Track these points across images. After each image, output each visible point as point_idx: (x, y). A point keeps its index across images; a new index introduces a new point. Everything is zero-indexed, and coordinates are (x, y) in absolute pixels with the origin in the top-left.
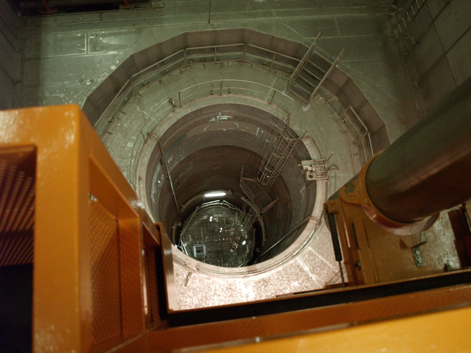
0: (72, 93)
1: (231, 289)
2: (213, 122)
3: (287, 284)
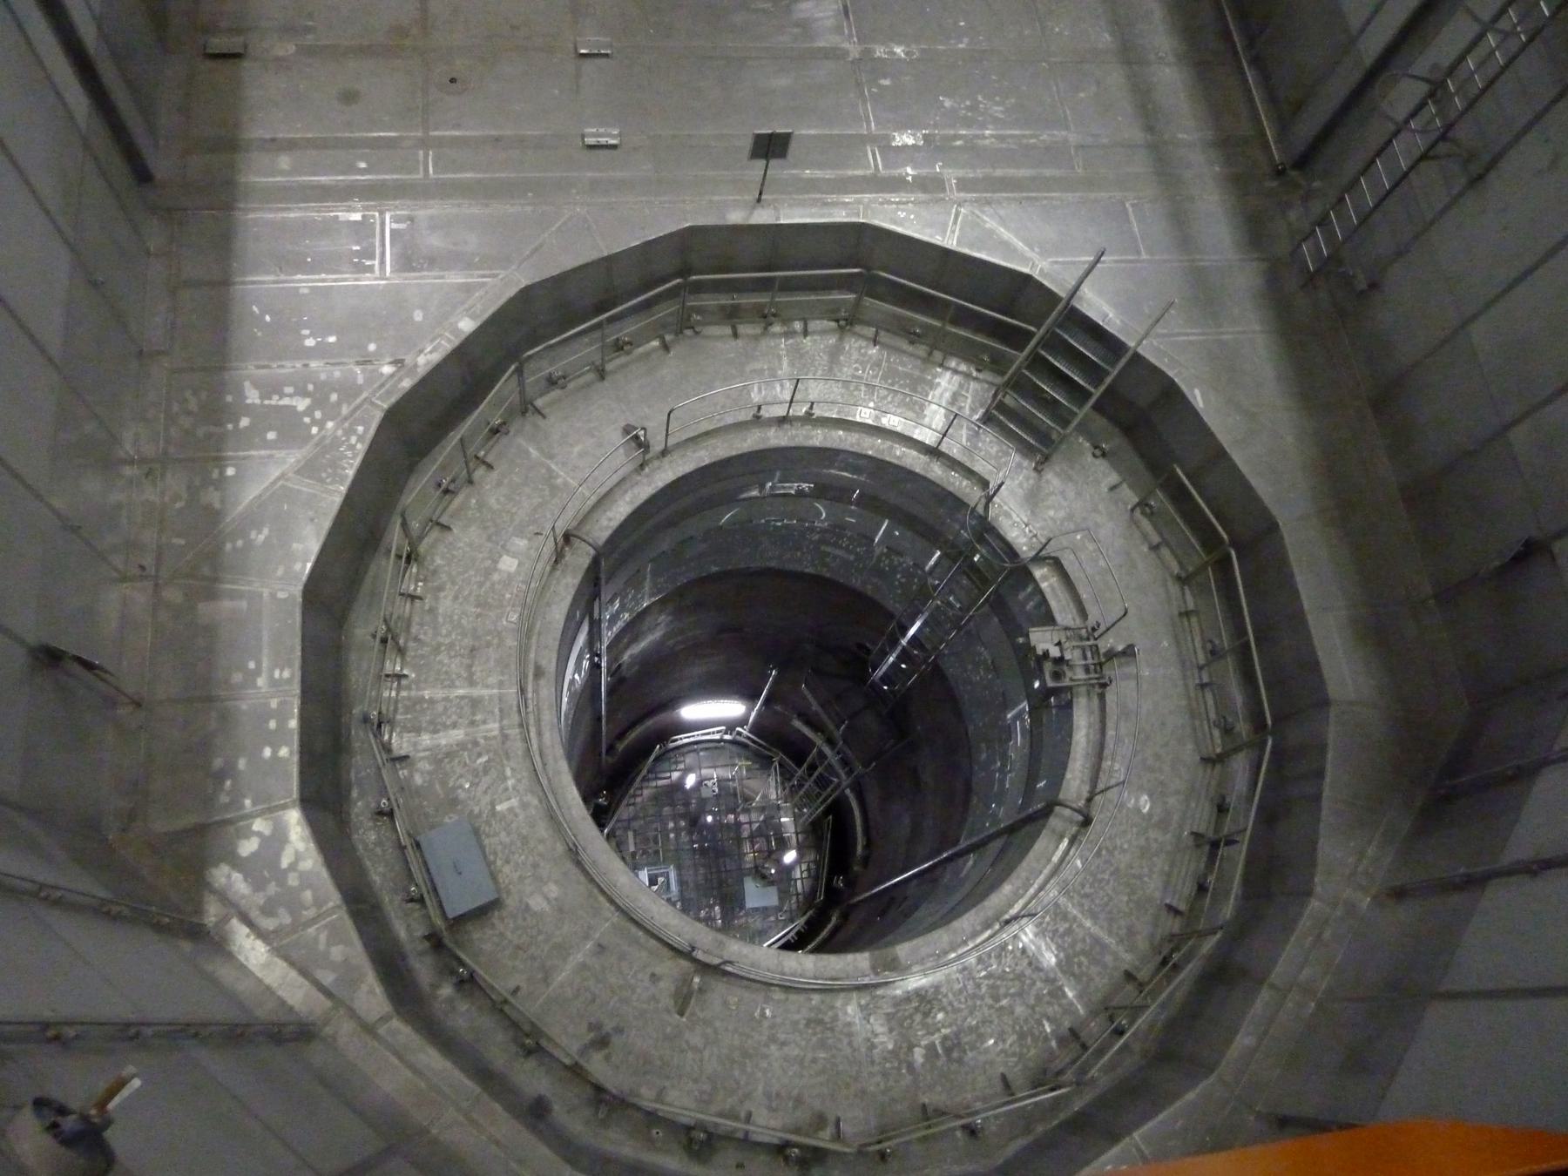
0: (334, 397)
1: (820, 1022)
2: (750, 498)
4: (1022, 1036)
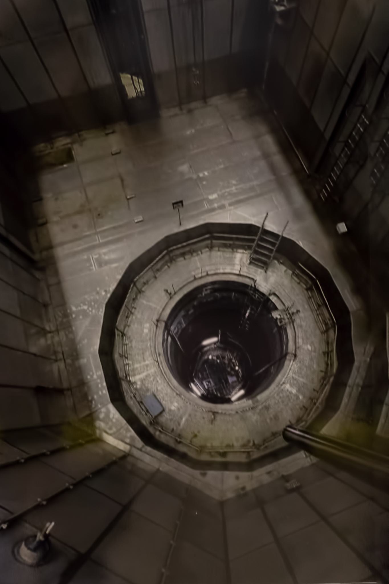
0: (93, 303)
4: (291, 410)
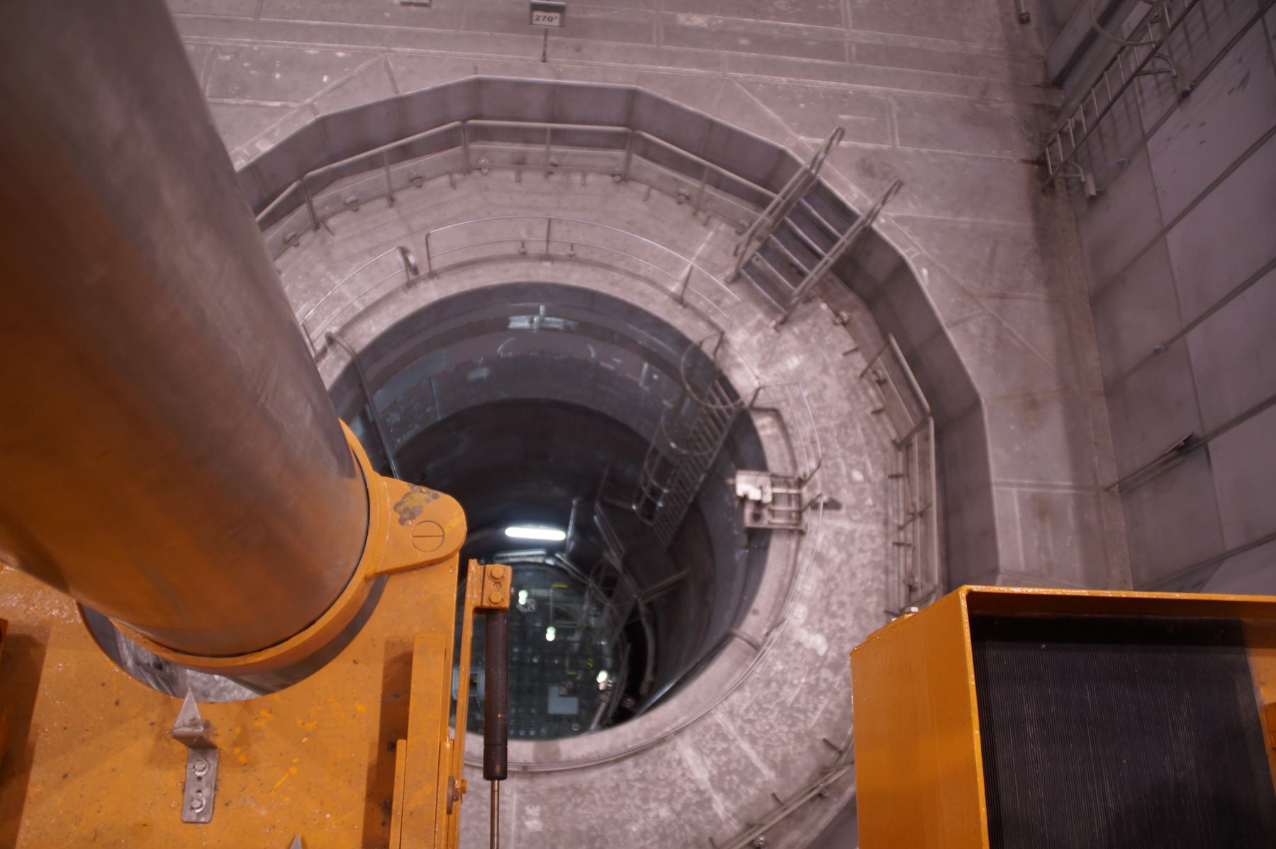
3: (638, 807)
